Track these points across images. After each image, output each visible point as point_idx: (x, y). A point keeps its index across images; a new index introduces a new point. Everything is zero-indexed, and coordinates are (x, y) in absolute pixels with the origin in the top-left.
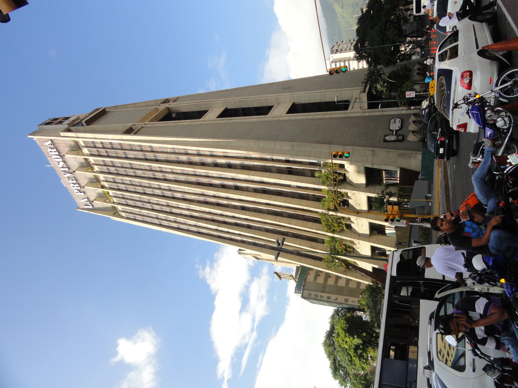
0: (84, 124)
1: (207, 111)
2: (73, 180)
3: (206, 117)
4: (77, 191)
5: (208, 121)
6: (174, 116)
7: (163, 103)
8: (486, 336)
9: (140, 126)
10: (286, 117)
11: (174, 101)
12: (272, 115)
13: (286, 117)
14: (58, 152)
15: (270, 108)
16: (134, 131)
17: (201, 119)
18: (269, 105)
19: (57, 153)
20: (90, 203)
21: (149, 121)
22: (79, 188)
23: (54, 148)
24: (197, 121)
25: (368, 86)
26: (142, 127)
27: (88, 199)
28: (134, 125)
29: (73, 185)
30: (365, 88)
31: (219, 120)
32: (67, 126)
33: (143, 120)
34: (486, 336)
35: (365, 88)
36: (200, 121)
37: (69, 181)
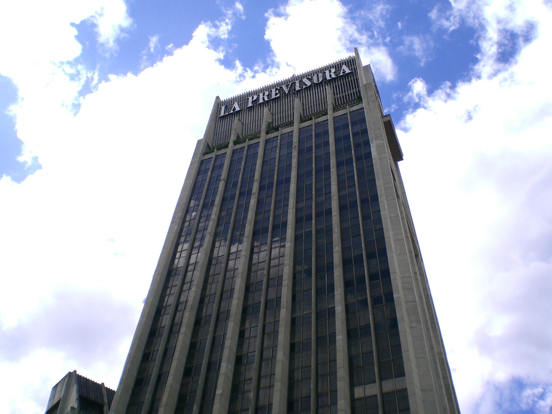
2: (276, 94)
22: (261, 101)
37: (273, 90)
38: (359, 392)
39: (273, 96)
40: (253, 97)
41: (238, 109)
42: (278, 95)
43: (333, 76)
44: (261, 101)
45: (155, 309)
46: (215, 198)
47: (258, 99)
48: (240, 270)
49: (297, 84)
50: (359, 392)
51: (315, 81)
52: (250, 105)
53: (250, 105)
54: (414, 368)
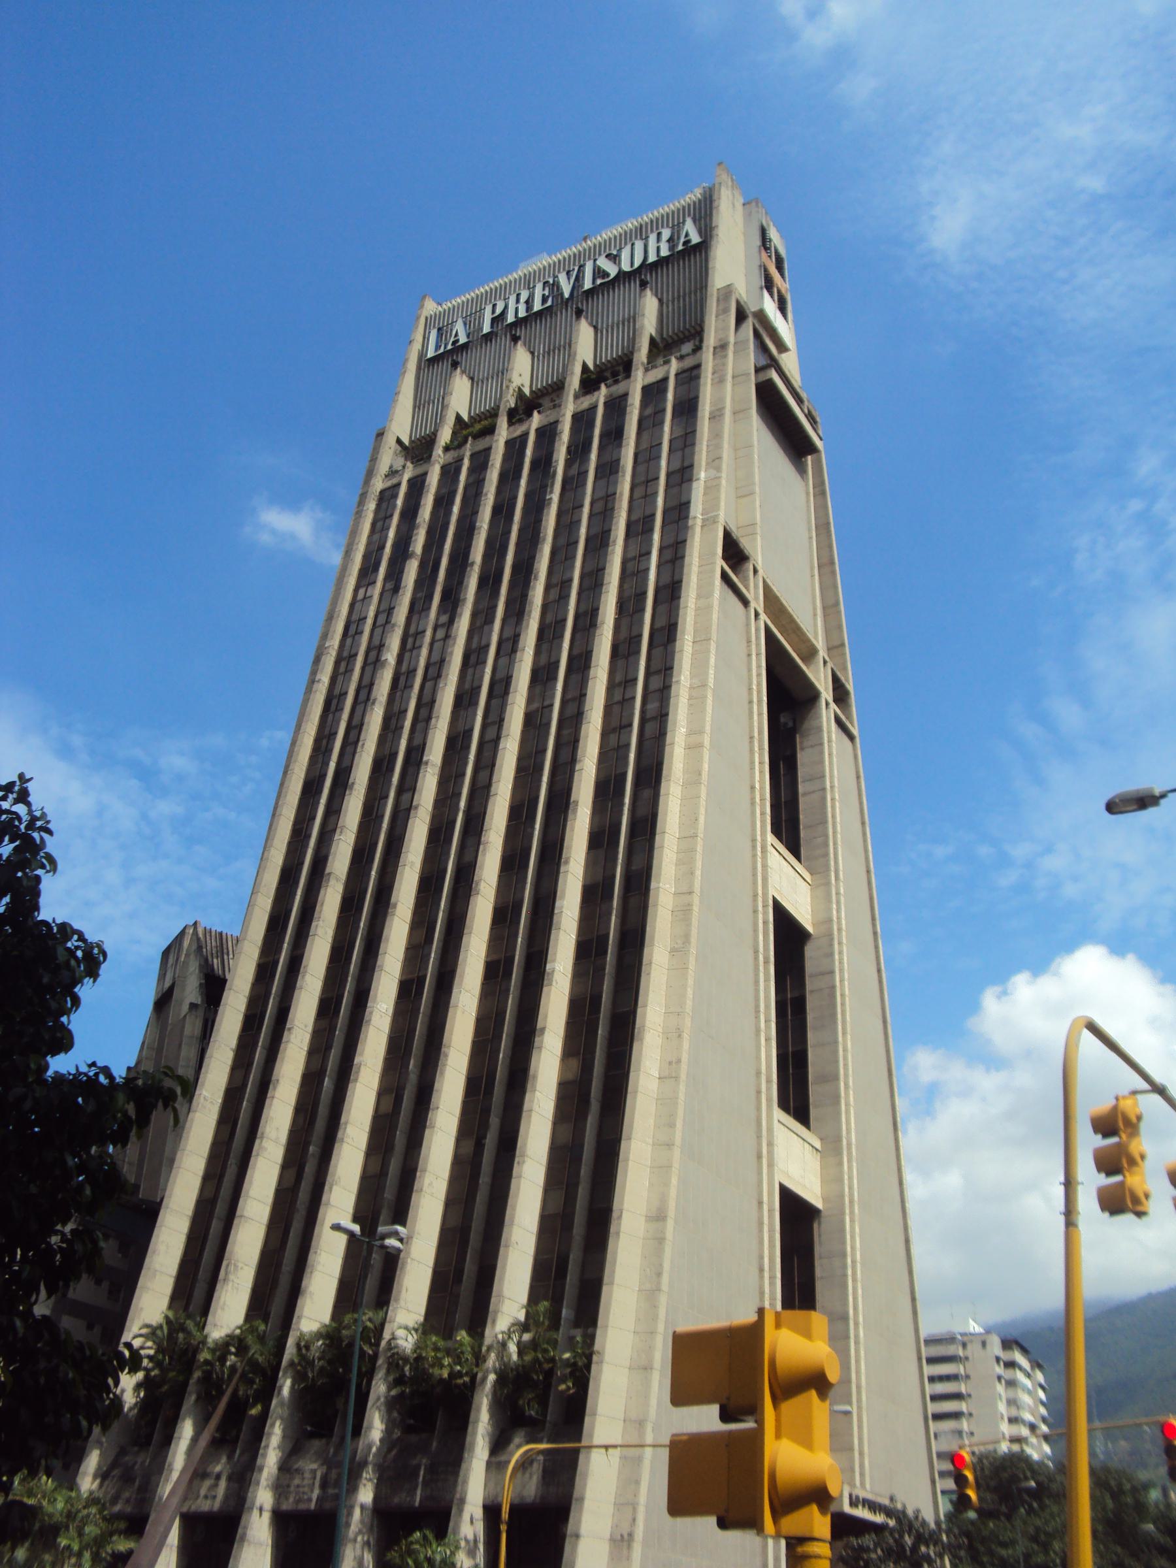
0: (763, 377)
1: (797, 856)
2: (544, 299)
3: (777, 859)
4: (498, 311)
5: (765, 866)
6: (783, 719)
7: (836, 680)
8: (10, 1497)
9: (749, 596)
10: (765, 894)
11: (838, 721)
12: (770, 848)
13: (765, 894)
14: (655, 265)
15: (801, 1114)
16: (734, 568)
17: (771, 838)
18: (813, 1112)
19: (652, 258)
20: (447, 353)
21: (768, 630)
22: (510, 318)
23: (671, 248)
24: (763, 822)
25: (879, 1519)
26: (745, 602)
27: (465, 346)
28: (755, 571)
29: (523, 298)
30: (873, 1506)
31: (765, 913)
32: (752, 307)
33: (772, 602)
34: (10, 1497)
35: (873, 1506)
36: (763, 834)
37: (539, 286)
38: (336, 1491)
39: (537, 306)
40: (494, 306)
41: (463, 339)
42: (549, 303)
43: (665, 252)
44: (510, 318)
45: (600, 1323)
46: (697, 389)
47: (504, 313)
48: (703, 468)
49: (459, 327)
50: (336, 1491)
51: (626, 267)
52: (486, 329)
53: (486, 329)
54: (705, 448)
